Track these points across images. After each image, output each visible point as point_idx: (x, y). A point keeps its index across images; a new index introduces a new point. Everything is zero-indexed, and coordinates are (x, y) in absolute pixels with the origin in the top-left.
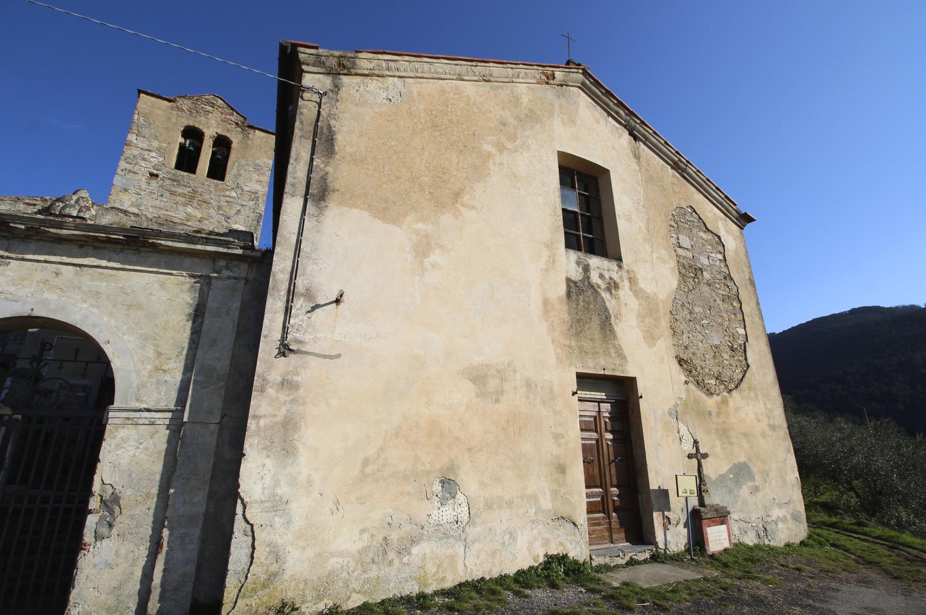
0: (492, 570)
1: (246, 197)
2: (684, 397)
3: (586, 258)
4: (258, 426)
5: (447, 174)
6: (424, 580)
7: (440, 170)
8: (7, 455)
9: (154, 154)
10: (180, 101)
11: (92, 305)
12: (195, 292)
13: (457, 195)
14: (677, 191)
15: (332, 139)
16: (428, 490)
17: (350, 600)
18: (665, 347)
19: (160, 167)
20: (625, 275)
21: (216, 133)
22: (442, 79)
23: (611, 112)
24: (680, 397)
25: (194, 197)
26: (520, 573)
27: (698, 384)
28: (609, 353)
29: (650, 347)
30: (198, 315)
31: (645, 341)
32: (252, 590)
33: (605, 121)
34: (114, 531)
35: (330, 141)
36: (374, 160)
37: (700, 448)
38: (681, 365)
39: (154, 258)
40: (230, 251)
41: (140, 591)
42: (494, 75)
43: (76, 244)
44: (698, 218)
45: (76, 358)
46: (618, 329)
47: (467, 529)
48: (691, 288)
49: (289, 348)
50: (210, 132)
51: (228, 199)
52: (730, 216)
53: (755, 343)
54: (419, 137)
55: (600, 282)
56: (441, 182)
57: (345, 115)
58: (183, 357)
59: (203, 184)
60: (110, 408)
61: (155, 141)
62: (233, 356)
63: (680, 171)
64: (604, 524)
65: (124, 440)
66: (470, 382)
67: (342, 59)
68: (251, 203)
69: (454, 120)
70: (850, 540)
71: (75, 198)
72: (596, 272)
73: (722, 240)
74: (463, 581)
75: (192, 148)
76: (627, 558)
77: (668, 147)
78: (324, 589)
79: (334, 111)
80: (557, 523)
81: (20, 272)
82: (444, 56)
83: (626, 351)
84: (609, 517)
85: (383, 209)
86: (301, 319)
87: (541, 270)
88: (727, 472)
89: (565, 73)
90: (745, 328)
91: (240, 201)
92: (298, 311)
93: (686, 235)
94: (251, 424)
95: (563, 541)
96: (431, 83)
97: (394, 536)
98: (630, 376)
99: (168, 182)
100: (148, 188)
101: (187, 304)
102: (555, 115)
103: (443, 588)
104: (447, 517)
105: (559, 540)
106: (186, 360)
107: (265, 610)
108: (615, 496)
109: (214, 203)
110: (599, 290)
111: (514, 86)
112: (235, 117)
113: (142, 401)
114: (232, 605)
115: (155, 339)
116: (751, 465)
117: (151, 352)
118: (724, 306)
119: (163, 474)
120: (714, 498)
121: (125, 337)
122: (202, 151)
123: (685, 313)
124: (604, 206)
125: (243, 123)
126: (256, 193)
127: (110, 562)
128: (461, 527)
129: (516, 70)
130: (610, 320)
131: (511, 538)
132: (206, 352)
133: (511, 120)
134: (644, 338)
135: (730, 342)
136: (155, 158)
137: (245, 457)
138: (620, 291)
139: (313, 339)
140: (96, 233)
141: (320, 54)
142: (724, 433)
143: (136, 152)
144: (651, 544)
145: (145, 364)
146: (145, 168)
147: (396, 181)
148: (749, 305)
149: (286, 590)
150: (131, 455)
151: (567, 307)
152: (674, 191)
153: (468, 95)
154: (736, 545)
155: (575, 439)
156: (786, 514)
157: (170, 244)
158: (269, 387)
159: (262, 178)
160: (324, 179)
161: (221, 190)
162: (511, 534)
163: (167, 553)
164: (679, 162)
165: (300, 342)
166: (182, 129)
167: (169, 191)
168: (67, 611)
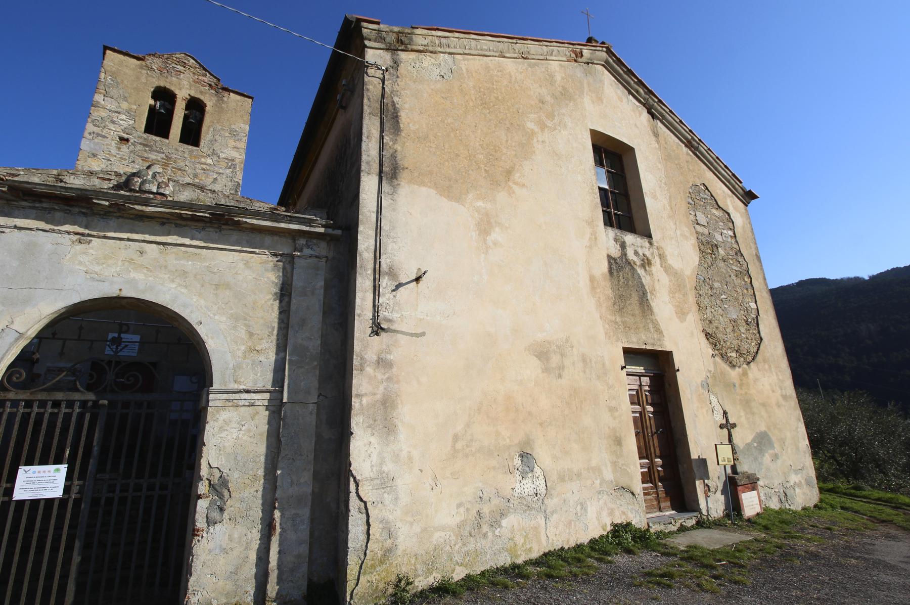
0: (569, 540)
1: (223, 165)
2: (712, 369)
3: (622, 236)
4: (361, 404)
5: (499, 152)
6: (515, 551)
7: (492, 148)
8: (95, 443)
9: (124, 117)
10: (149, 60)
11: (180, 285)
12: (279, 271)
13: (509, 173)
14: (691, 168)
15: (397, 117)
16: (510, 464)
17: (455, 573)
18: (693, 319)
19: (130, 131)
20: (656, 251)
21: (189, 95)
22: (486, 56)
23: (632, 90)
24: (709, 369)
25: (169, 164)
26: (593, 542)
27: (723, 357)
28: (648, 328)
29: (682, 322)
30: (285, 293)
31: (677, 316)
32: (371, 566)
33: (626, 100)
34: (226, 515)
35: (396, 118)
36: (435, 137)
37: (729, 418)
38: (708, 339)
39: (235, 236)
40: (312, 229)
41: (256, 574)
42: (531, 52)
43: (157, 222)
44: (710, 196)
45: (64, 344)
46: (653, 304)
47: (546, 501)
48: (710, 264)
49: (381, 327)
50: (182, 94)
51: (204, 166)
52: (736, 193)
53: (765, 317)
54: (472, 115)
55: (635, 259)
56: (494, 160)
57: (405, 91)
58: (274, 337)
59: (176, 150)
60: (210, 390)
61: (124, 102)
62: (322, 336)
63: (693, 149)
64: (653, 493)
65: (227, 422)
66: (536, 359)
67: (400, 35)
68: (228, 171)
69: (500, 98)
70: (855, 503)
71: (151, 173)
72: (631, 249)
73: (732, 217)
74: (547, 551)
75: (162, 111)
76: (678, 525)
77: (682, 125)
78: (432, 563)
79: (396, 88)
80: (618, 494)
81: (103, 251)
82: (489, 33)
83: (662, 326)
84: (656, 487)
85: (447, 187)
86: (388, 297)
87: (586, 247)
88: (751, 442)
89: (591, 51)
90: (756, 302)
91: (216, 169)
92: (384, 290)
93: (702, 212)
94: (355, 403)
95: (625, 510)
96: (477, 60)
97: (486, 510)
98: (667, 350)
99: (139, 147)
100: (118, 154)
101: (273, 283)
102: (585, 93)
103: (531, 559)
104: (528, 490)
105: (622, 509)
106: (278, 340)
107: (384, 585)
108: (659, 467)
109: (189, 171)
110: (635, 266)
111: (548, 64)
112: (208, 79)
113: (240, 383)
114: (355, 582)
115: (245, 319)
116: (770, 434)
117: (243, 332)
118: (738, 281)
119: (267, 456)
120: (745, 467)
121: (217, 317)
122: (174, 115)
123: (707, 288)
124: (630, 183)
125: (216, 85)
126: (233, 160)
127: (224, 546)
128: (541, 499)
129: (550, 47)
130: (647, 296)
131: (582, 508)
132: (297, 332)
133: (548, 98)
134: (676, 313)
135: (745, 316)
136: (125, 121)
137: (353, 435)
138: (653, 267)
139: (400, 317)
140: (176, 209)
141: (381, 30)
142: (746, 403)
143: (104, 114)
144: (694, 511)
145: (238, 344)
146: (114, 131)
147: (456, 159)
148: (758, 281)
149: (400, 565)
150: (235, 437)
151: (610, 283)
152: (689, 169)
153: (510, 72)
154: (765, 510)
155: (627, 412)
156: (801, 479)
157: (255, 222)
158: (367, 365)
159: (239, 144)
160: (394, 157)
161: (195, 157)
162: (582, 504)
163: (281, 534)
164: (692, 141)
165: (389, 321)
166: (152, 90)
167: (141, 157)
168: (186, 600)
